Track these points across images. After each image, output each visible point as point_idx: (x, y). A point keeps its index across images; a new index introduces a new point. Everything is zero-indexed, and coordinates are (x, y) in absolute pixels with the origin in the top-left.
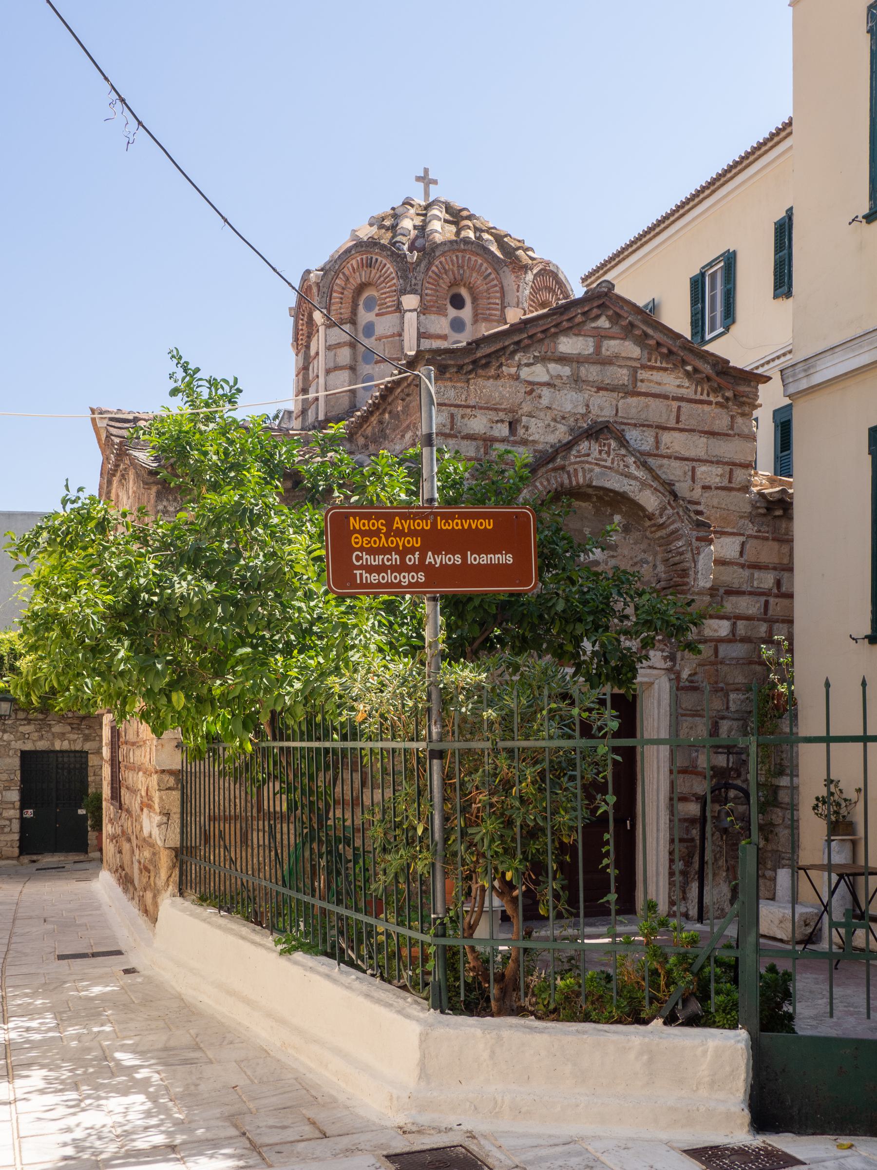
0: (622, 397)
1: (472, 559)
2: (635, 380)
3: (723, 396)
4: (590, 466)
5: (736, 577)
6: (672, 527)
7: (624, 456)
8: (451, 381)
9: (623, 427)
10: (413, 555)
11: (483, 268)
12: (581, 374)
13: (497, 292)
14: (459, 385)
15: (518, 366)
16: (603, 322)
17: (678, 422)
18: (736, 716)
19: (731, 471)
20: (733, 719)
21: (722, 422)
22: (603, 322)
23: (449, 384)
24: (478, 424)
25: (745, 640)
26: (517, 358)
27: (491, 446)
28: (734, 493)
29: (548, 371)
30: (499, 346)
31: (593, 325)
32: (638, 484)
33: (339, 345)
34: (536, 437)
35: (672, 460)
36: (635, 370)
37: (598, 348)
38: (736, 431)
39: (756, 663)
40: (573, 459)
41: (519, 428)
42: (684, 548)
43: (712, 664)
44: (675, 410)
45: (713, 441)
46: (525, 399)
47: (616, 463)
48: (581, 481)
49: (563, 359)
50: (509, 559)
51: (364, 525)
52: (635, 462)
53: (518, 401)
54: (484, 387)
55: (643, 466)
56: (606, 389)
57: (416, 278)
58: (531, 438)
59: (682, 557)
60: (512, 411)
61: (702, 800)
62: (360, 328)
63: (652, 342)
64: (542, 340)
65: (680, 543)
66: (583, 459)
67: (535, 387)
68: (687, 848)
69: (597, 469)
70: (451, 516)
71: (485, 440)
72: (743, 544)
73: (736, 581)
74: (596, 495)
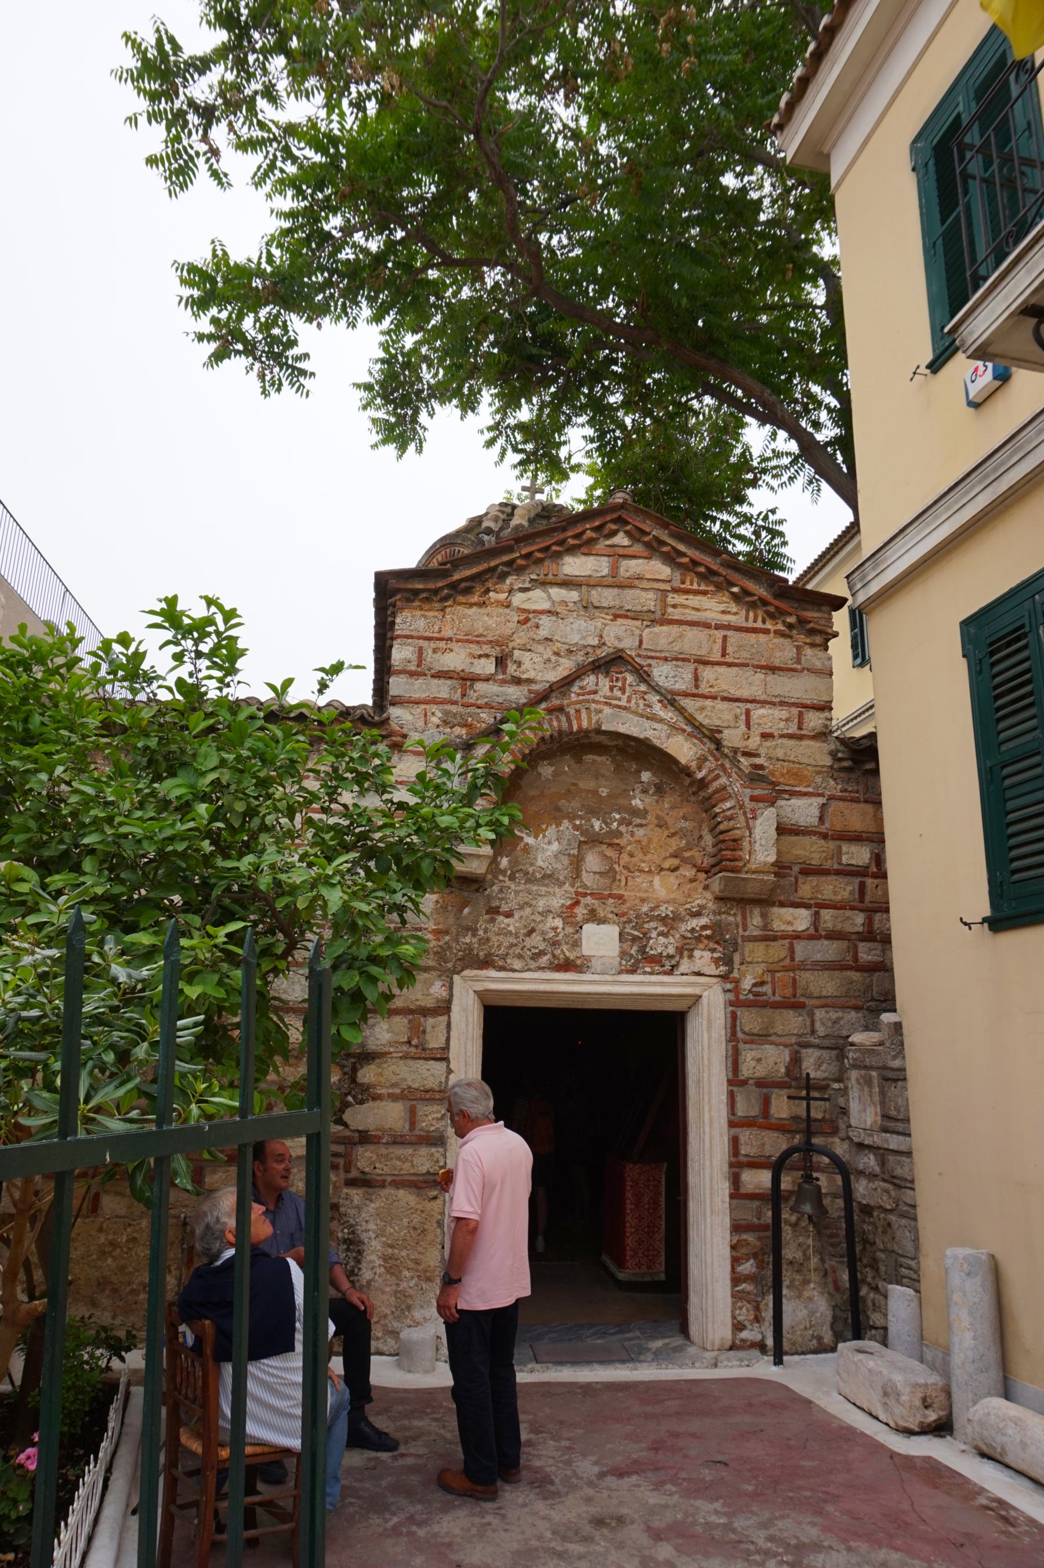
4: (598, 707)
5: (813, 851)
9: (650, 661)
14: (431, 614)
18: (827, 1043)
19: (801, 715)
20: (822, 1048)
21: (784, 651)
23: (419, 613)
24: (455, 659)
25: (834, 935)
26: (508, 581)
27: (472, 687)
28: (805, 743)
29: (549, 596)
30: (484, 566)
31: (608, 542)
32: (666, 727)
34: (531, 675)
35: (718, 701)
37: (614, 570)
38: (804, 664)
39: (850, 968)
43: (786, 969)
44: (720, 641)
47: (633, 701)
49: (567, 583)
55: (672, 705)
56: (626, 617)
58: (525, 676)
61: (777, 1168)
65: (728, 805)
67: (531, 616)
68: (760, 1239)
69: (607, 710)
72: (823, 807)
73: (816, 856)
74: (616, 746)
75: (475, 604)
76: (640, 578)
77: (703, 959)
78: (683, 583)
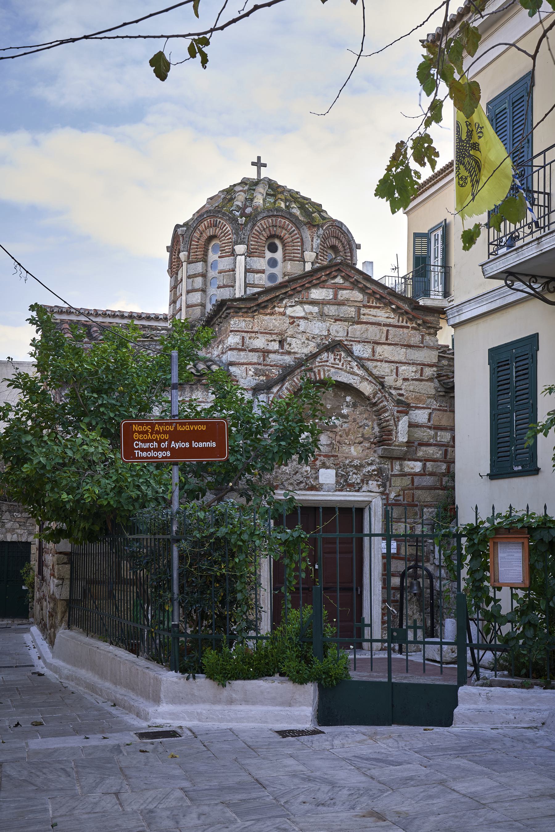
0: (351, 325)
1: (194, 445)
2: (359, 314)
3: (416, 323)
4: (328, 368)
6: (381, 404)
7: (350, 361)
8: (243, 317)
9: (351, 343)
10: (165, 443)
11: (290, 227)
12: (325, 311)
13: (299, 242)
14: (248, 319)
15: (285, 307)
16: (339, 280)
17: (387, 339)
19: (422, 369)
21: (416, 338)
22: (339, 280)
23: (242, 319)
24: (259, 342)
25: (431, 474)
26: (284, 302)
27: (268, 356)
28: (423, 383)
29: (304, 309)
30: (273, 295)
31: (333, 282)
32: (359, 378)
33: (195, 276)
34: (296, 350)
36: (359, 309)
37: (336, 295)
38: (425, 344)
39: (438, 489)
40: (317, 364)
41: (285, 344)
42: (389, 418)
45: (409, 350)
46: (289, 327)
47: (345, 366)
48: (322, 377)
49: (313, 303)
50: (214, 445)
51: (140, 428)
52: (357, 365)
53: (284, 328)
54: (263, 320)
55: (362, 367)
56: (341, 320)
57: (244, 234)
58: (292, 351)
59: (388, 423)
60: (280, 334)
62: (209, 265)
63: (369, 291)
64: (300, 291)
65: (387, 415)
66: (323, 364)
67: (295, 320)
69: (333, 370)
70: (184, 424)
71: (263, 352)
72: (430, 414)
75: (269, 314)
76: (348, 300)
77: (373, 485)
78: (368, 302)
